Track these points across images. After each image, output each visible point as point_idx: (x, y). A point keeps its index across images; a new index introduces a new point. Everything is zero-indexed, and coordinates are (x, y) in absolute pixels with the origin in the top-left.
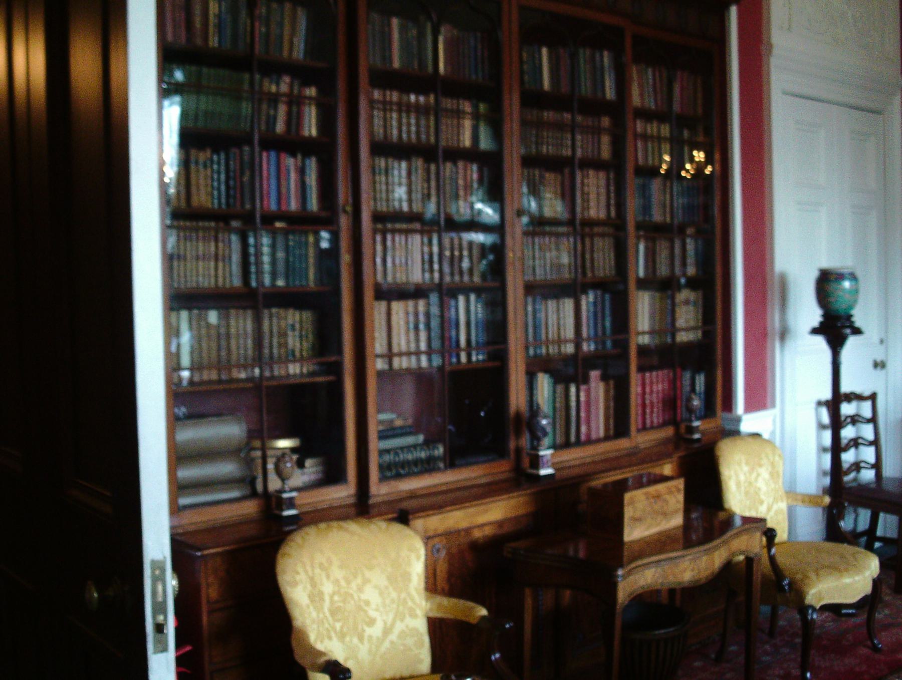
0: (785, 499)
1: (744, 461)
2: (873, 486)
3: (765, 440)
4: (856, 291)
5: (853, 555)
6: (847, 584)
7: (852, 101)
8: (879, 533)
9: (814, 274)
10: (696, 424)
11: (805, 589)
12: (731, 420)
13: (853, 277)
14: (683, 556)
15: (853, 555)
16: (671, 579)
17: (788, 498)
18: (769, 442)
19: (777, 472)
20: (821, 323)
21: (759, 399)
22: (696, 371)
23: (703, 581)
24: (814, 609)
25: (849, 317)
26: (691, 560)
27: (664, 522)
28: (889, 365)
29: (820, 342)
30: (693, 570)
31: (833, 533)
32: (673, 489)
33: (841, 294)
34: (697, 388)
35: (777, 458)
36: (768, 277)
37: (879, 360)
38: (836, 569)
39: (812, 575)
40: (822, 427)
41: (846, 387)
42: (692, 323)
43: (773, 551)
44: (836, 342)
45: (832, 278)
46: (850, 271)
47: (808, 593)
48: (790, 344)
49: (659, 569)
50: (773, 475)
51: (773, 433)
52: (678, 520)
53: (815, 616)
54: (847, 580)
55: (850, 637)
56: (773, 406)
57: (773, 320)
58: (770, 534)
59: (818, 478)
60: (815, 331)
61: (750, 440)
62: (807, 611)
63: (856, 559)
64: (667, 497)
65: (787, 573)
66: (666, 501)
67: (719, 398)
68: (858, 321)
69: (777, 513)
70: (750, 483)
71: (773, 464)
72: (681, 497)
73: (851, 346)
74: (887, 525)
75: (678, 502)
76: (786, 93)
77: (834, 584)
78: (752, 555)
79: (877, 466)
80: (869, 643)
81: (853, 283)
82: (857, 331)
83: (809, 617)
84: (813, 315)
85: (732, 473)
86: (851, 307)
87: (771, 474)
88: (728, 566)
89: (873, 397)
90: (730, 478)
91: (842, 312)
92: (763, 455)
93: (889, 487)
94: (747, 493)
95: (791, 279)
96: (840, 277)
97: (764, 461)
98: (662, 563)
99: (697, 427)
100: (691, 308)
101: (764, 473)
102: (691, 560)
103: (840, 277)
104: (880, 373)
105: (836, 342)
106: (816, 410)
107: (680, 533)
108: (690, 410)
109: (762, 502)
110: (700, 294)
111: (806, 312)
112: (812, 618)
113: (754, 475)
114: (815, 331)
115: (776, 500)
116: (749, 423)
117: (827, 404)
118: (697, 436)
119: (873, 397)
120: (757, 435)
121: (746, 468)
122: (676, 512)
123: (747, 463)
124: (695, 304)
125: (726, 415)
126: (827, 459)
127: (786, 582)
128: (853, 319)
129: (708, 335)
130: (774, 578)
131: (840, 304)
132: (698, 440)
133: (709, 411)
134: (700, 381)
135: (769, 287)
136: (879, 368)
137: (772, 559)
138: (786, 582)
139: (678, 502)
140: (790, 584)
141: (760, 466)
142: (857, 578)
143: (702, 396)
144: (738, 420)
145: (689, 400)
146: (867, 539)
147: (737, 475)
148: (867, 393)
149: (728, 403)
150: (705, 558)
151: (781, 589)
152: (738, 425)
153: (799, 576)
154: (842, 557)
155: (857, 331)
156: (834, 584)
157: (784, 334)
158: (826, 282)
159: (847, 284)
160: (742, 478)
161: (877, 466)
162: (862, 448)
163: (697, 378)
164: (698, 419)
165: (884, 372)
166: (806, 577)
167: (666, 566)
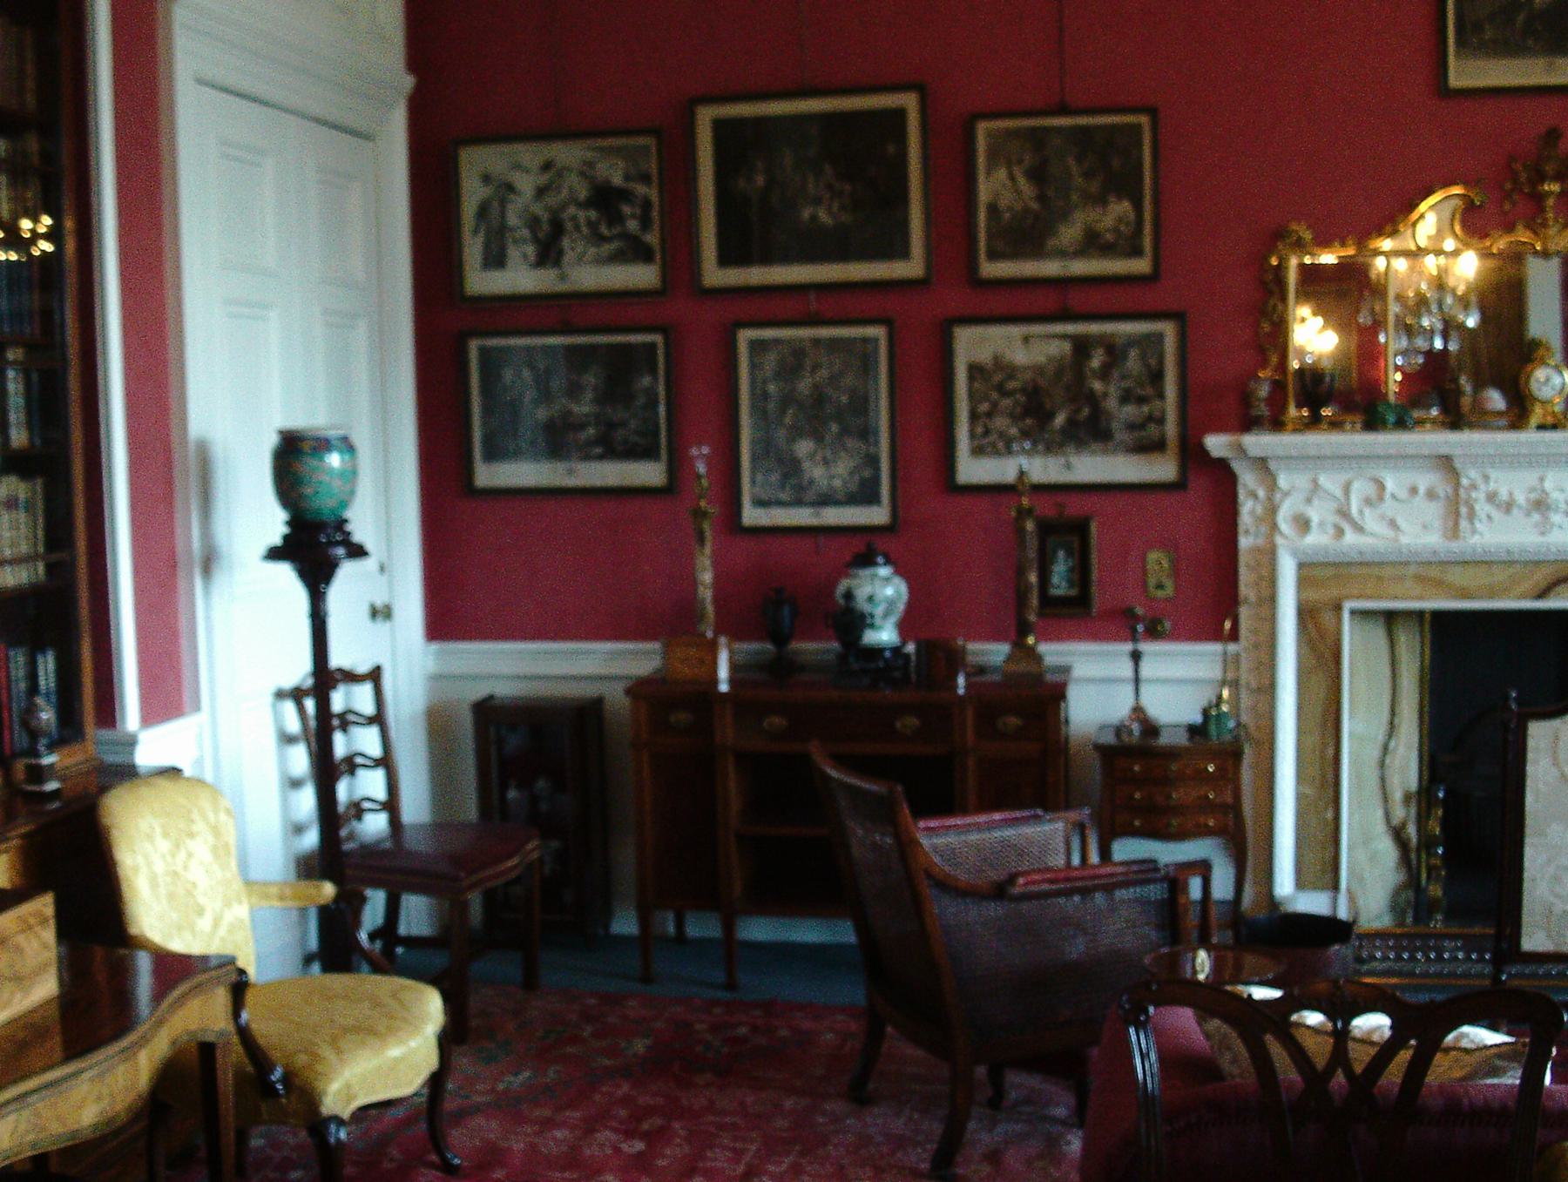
0: (245, 899)
1: (158, 830)
2: (388, 845)
3: (188, 779)
4: (351, 474)
5: (394, 995)
6: (397, 1060)
7: (316, 109)
8: (403, 930)
9: (271, 441)
10: (48, 760)
11: (320, 1085)
12: (117, 743)
13: (347, 446)
14: (81, 1072)
15: (394, 995)
16: (56, 1128)
17: (250, 895)
18: (199, 782)
19: (227, 845)
20: (286, 538)
21: (169, 696)
22: (35, 648)
23: (123, 1117)
24: (340, 1122)
25: (341, 523)
26: (92, 1080)
27: (18, 996)
28: (396, 612)
29: (285, 573)
30: (99, 1098)
31: (335, 946)
32: (32, 921)
33: (326, 478)
34: (42, 682)
35: (223, 817)
36: (175, 445)
37: (379, 603)
38: (371, 1031)
39: (326, 1052)
40: (287, 739)
41: (338, 658)
42: (24, 548)
43: (245, 1016)
44: (317, 576)
45: (306, 447)
46: (341, 432)
47: (325, 1093)
48: (220, 579)
49: (26, 1113)
50: (218, 851)
51: (199, 762)
52: (47, 987)
53: (343, 1135)
54: (395, 1052)
55: (394, 1152)
56: (197, 707)
57: (189, 538)
58: (239, 987)
59: (286, 840)
60: (274, 554)
61: (163, 783)
62: (327, 1128)
63: (403, 1005)
64: (21, 939)
65: (275, 1055)
66: (19, 950)
67: (87, 698)
68: (362, 528)
69: (232, 928)
70: (175, 873)
71: (216, 831)
72: (49, 934)
73: (350, 587)
74: (417, 916)
75: (45, 946)
76: (201, 82)
77: (375, 1062)
78: (210, 1038)
79: (391, 806)
80: (434, 1158)
81: (347, 457)
82: (358, 552)
83: (332, 1140)
84: (274, 524)
85: (140, 860)
86: (345, 504)
87: (215, 850)
88: (169, 1075)
89: (375, 676)
90: (136, 869)
91: (327, 515)
92: (195, 815)
93: (416, 843)
94: (171, 896)
95: (218, 453)
96: (323, 445)
97: (199, 826)
98: (30, 1100)
99: (52, 765)
100: (22, 516)
101: (201, 846)
102: (92, 1080)
103: (323, 445)
104: (382, 627)
105: (317, 576)
106: (274, 706)
107: (54, 1012)
108: (34, 734)
109: (200, 912)
110: (39, 483)
111: (253, 517)
112: (338, 1140)
113: (182, 855)
114: (274, 554)
115: (227, 903)
116: (153, 746)
117: (297, 695)
118: (52, 786)
119: (375, 676)
120: (173, 772)
121: (164, 845)
122: (40, 970)
123: (166, 835)
124: (29, 507)
125: (105, 734)
126: (306, 801)
127: (277, 1074)
128: (349, 527)
129: (60, 571)
130: (250, 1069)
131: (322, 501)
132: (55, 794)
133: (69, 729)
134: (47, 666)
135: (177, 472)
136: (379, 619)
137: (244, 1033)
138: (277, 1074)
139: (45, 946)
140: (287, 1079)
141: (191, 835)
142: (413, 1044)
143: (53, 698)
144: (131, 742)
145: (31, 710)
146: (394, 955)
147: (149, 864)
148: (363, 668)
149: (108, 711)
150: (121, 1068)
151: (268, 1090)
152: (132, 754)
153: (301, 1059)
154: (376, 1004)
155: (358, 552)
156: (375, 1062)
157: (209, 562)
158: (293, 456)
159: (334, 460)
160: (159, 868)
161: (391, 806)
162: (361, 773)
163: (40, 659)
164: (52, 748)
165: (388, 624)
166: (316, 1057)
167: (40, 1104)
